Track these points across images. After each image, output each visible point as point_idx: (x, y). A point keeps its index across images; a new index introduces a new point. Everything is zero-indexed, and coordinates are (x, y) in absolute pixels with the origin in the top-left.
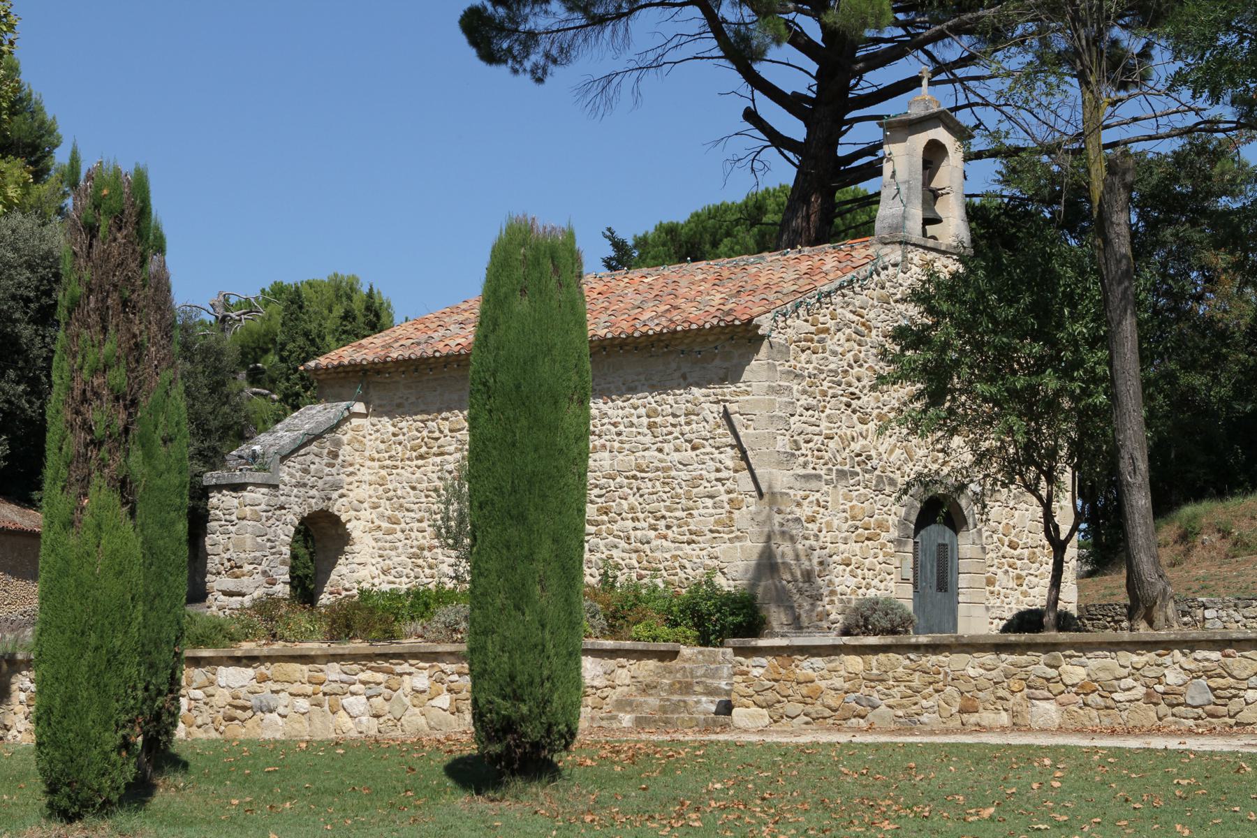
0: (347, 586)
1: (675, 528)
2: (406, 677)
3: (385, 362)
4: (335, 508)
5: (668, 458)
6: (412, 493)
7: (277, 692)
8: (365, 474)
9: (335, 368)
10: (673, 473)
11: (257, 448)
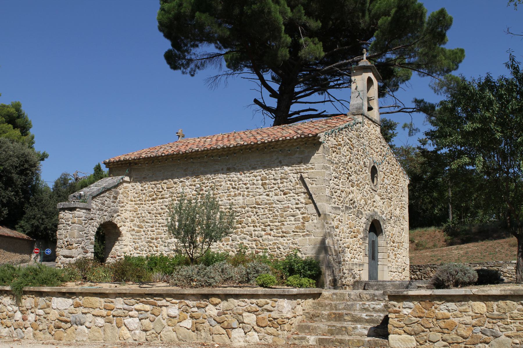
0: (119, 254)
1: (275, 230)
2: (164, 308)
3: (139, 159)
4: (115, 221)
5: (272, 199)
6: (149, 215)
7: (85, 313)
8: (128, 207)
9: (117, 162)
10: (274, 205)
11: (82, 193)
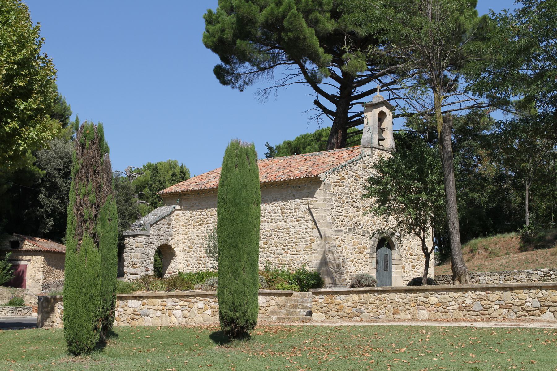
2: (195, 303)
3: (187, 191)
5: (288, 225)
7: (149, 309)
10: (290, 230)
11: (142, 222)
